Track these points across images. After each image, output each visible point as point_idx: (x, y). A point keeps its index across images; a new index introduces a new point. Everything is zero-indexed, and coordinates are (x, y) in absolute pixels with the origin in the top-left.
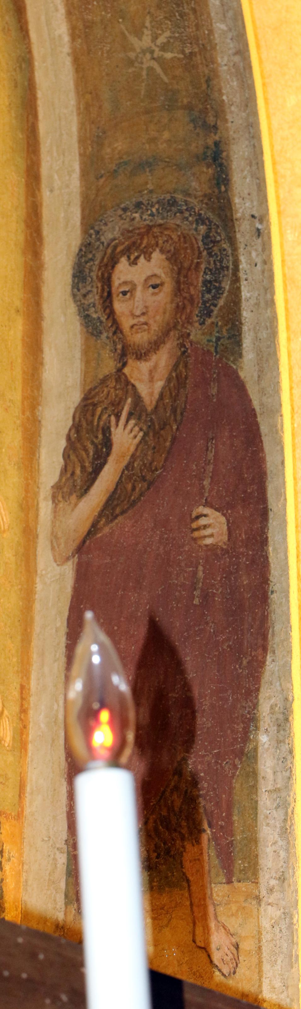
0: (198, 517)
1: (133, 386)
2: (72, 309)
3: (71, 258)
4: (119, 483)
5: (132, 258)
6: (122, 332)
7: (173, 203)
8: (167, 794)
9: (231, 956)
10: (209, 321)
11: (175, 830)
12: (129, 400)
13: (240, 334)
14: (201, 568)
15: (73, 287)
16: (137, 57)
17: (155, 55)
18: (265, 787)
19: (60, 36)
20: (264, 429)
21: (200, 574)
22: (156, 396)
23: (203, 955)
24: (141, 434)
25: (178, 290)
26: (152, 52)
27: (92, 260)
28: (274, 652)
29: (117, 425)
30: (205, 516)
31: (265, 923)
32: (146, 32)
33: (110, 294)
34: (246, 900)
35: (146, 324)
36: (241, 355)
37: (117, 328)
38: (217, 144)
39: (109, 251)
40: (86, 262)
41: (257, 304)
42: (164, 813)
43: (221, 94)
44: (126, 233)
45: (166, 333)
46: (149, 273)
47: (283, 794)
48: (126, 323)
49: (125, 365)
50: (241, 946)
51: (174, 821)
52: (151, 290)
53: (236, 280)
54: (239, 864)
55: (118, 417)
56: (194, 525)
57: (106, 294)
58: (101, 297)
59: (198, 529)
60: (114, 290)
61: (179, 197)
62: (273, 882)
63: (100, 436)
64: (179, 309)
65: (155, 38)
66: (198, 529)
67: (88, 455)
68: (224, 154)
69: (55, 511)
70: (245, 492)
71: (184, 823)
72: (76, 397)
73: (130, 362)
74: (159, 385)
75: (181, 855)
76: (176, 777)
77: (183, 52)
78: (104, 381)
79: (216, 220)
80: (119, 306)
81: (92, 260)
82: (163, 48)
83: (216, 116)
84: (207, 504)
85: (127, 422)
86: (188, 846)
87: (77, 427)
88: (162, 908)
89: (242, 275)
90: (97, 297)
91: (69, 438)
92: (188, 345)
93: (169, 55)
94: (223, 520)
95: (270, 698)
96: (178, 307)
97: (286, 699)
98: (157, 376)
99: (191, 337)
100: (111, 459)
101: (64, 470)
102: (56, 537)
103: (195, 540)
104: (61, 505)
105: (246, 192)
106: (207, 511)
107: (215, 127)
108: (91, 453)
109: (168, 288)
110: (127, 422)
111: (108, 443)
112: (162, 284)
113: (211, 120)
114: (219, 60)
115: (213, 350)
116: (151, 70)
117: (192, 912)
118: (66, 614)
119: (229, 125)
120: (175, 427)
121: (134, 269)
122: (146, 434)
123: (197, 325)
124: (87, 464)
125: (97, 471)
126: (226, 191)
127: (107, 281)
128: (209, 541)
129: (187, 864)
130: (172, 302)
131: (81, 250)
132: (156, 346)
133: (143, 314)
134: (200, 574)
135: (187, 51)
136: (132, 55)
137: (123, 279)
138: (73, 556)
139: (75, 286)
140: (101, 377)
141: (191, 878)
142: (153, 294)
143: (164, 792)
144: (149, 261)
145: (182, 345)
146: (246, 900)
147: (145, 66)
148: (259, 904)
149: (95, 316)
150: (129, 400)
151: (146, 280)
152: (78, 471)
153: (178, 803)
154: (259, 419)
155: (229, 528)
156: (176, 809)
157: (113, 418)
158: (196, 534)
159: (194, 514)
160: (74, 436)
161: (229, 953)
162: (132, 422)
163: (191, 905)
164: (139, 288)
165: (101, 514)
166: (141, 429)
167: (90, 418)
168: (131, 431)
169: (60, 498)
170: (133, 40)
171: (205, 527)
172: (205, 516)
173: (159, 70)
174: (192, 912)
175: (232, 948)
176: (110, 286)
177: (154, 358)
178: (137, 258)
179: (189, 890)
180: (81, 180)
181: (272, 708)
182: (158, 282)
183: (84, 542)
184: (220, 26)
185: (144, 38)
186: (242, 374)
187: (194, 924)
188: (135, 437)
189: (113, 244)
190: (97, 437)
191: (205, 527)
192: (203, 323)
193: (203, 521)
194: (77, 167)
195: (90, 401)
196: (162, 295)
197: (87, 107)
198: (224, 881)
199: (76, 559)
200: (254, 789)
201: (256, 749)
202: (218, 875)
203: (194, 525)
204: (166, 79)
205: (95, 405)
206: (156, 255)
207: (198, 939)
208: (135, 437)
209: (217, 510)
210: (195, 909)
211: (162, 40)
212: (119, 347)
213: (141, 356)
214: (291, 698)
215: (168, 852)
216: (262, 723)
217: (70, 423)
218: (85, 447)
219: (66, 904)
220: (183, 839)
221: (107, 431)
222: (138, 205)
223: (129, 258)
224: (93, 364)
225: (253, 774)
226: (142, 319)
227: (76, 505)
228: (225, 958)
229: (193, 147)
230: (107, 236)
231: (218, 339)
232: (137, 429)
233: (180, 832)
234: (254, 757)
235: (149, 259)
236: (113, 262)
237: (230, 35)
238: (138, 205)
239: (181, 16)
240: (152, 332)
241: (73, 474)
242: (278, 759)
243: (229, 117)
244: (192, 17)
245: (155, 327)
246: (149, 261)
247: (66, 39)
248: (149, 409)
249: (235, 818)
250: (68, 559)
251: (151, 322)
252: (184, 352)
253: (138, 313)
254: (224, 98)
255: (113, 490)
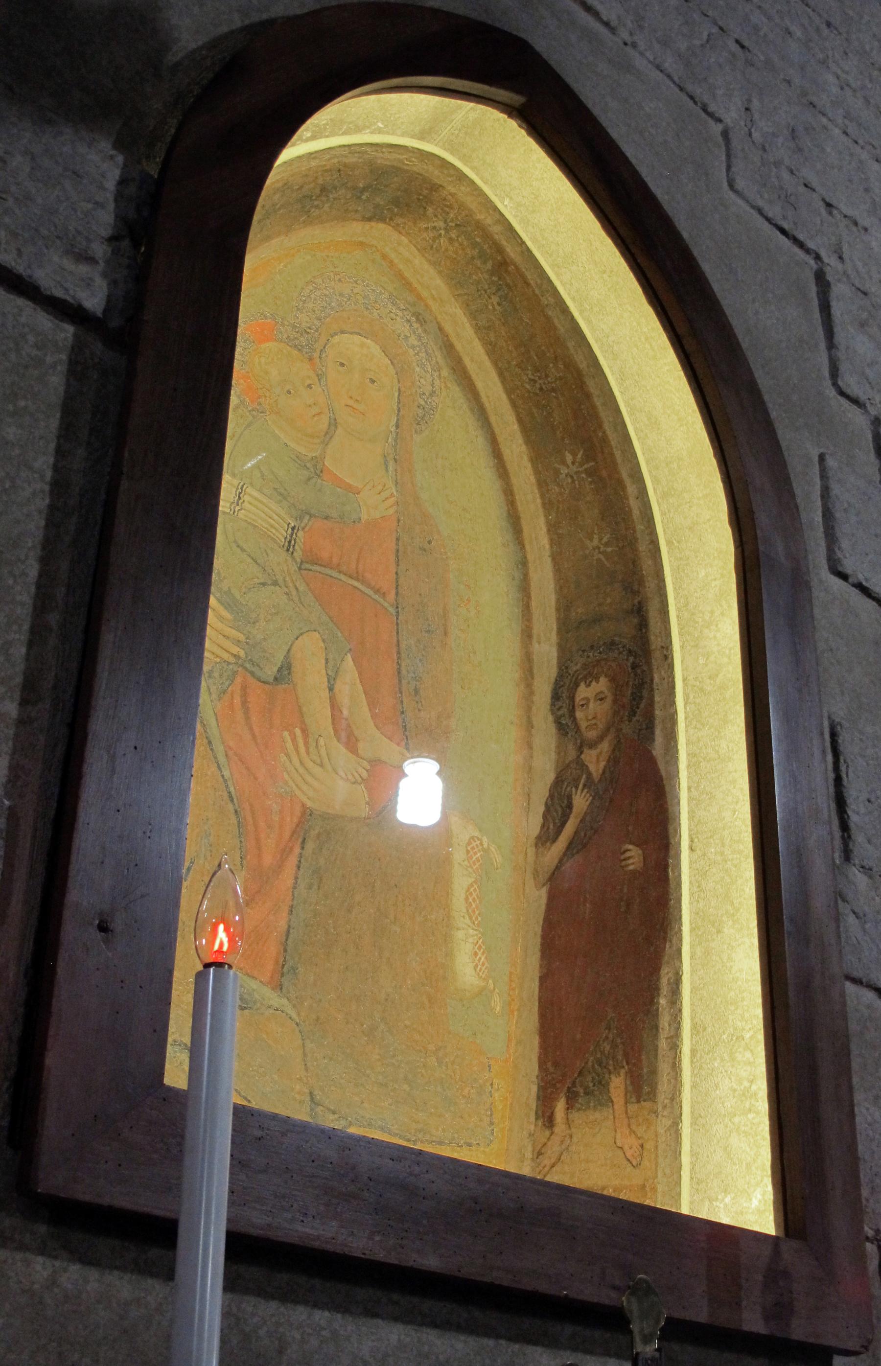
0: (625, 852)
1: (587, 766)
2: (551, 718)
3: (551, 685)
4: (576, 833)
5: (588, 682)
6: (580, 732)
7: (613, 643)
8: (601, 1042)
9: (638, 1152)
10: (634, 719)
11: (605, 1067)
12: (584, 776)
13: (654, 727)
14: (626, 886)
15: (551, 705)
16: (590, 553)
17: (601, 550)
18: (663, 1035)
19: (544, 546)
20: (667, 789)
21: (625, 890)
22: (601, 771)
23: (620, 1153)
24: (591, 798)
25: (615, 701)
26: (599, 548)
27: (563, 686)
28: (671, 941)
29: (576, 794)
30: (629, 850)
31: (661, 1131)
32: (595, 536)
33: (574, 707)
34: (648, 1114)
35: (595, 724)
36: (654, 740)
37: (578, 729)
38: (639, 603)
39: (574, 679)
40: (560, 688)
41: (664, 705)
42: (599, 1056)
43: (642, 570)
44: (585, 666)
45: (608, 729)
46: (599, 690)
47: (674, 1040)
48: (583, 725)
49: (582, 753)
50: (644, 1145)
51: (604, 1061)
52: (599, 702)
53: (652, 690)
54: (646, 1089)
55: (577, 788)
56: (622, 857)
57: (571, 708)
58: (568, 709)
59: (624, 860)
60: (576, 703)
61: (617, 639)
62: (667, 1101)
63: (566, 802)
64: (616, 713)
65: (601, 540)
66: (624, 860)
67: (557, 812)
68: (644, 608)
69: (537, 854)
70: (464, 1097)
71: (611, 1062)
72: (551, 777)
73: (585, 750)
74: (602, 764)
75: (608, 1084)
76: (607, 1031)
77: (617, 546)
78: (568, 766)
79: (640, 653)
80: (579, 714)
81: (563, 686)
82: (607, 544)
83: (639, 585)
84: (631, 843)
85: (582, 790)
86: (613, 1077)
87: (551, 796)
88: (596, 1121)
89: (655, 687)
90: (566, 710)
91: (546, 804)
92: (621, 736)
93: (609, 549)
94: (640, 852)
95: (668, 973)
96: (615, 711)
97: (677, 973)
98: (601, 759)
99: (624, 731)
100: (572, 816)
101: (543, 826)
102: (537, 871)
103: (622, 867)
104: (540, 850)
105: (658, 631)
106: (630, 847)
107: (639, 592)
108: (560, 813)
109: (609, 700)
110: (582, 790)
111: (570, 806)
112: (606, 697)
113: (636, 587)
114: (640, 548)
115: (636, 738)
116: (599, 560)
117: (614, 1122)
118: (541, 923)
119: (647, 589)
120: (611, 792)
121: (589, 689)
122: (594, 799)
123: (627, 722)
124: (557, 821)
125: (563, 824)
126: (646, 633)
127: (572, 698)
128: (631, 868)
129: (612, 1090)
130: (612, 708)
131: (556, 680)
132: (601, 738)
133: (594, 718)
134: (625, 890)
135: (621, 545)
136: (587, 552)
137: (582, 696)
138: (546, 883)
139: (553, 704)
140: (567, 762)
141: (614, 1100)
142: (600, 705)
143: (599, 1041)
144: (598, 683)
145: (618, 736)
146: (648, 1114)
147: (595, 558)
148: (657, 1117)
149: (564, 722)
150: (584, 776)
151: (597, 694)
152: (551, 826)
153: (608, 1048)
154: (665, 782)
155: (644, 857)
156: (606, 1052)
157: (574, 789)
158: (623, 863)
159: (622, 850)
160: (549, 802)
161: (637, 1150)
162: (586, 790)
163: (614, 1118)
164: (592, 701)
165: (565, 854)
166: (591, 795)
167: (559, 790)
168: (585, 796)
169: (540, 845)
170: (588, 542)
171: (629, 858)
172: (629, 850)
173: (603, 559)
174: (614, 1122)
175: (639, 1147)
176: (574, 702)
177: (600, 746)
178: (591, 682)
179: (613, 1109)
180: (557, 635)
181: (669, 980)
182: (603, 696)
183: (553, 873)
184: (640, 527)
185: (594, 540)
186: (654, 753)
187: (616, 1131)
188: (587, 800)
189: (576, 674)
190: (563, 802)
191: (629, 858)
192: (630, 721)
193: (628, 854)
194: (555, 627)
195: (560, 779)
196: (605, 704)
197: (561, 588)
198: (635, 1101)
199: (548, 885)
200: (656, 1036)
201: (657, 1010)
202: (631, 1097)
203: (622, 857)
204: (608, 565)
205: (563, 781)
206: (603, 680)
207: (618, 1141)
208: (587, 800)
209: (637, 846)
210: (616, 1120)
211: (605, 540)
212: (579, 741)
213: (592, 745)
214: (681, 973)
215: (600, 1082)
216: (662, 991)
217: (547, 795)
218: (555, 810)
219: (537, 1119)
220: (610, 1073)
221: (570, 798)
222: (592, 647)
223: (586, 682)
224: (562, 754)
225: (656, 1027)
226: (593, 722)
227: (549, 849)
228: (635, 1154)
229: (625, 607)
230: (574, 668)
231: (640, 730)
232: (588, 795)
233: (608, 1069)
234: (656, 1015)
235: (598, 682)
236: (577, 685)
237: (646, 532)
238: (592, 647)
239: (616, 523)
240: (599, 729)
241: (548, 828)
242: (672, 1016)
243: (647, 584)
244: (623, 524)
245: (601, 726)
246: (598, 683)
247: (547, 547)
248: (596, 781)
249: (643, 1057)
250: (544, 885)
251: (599, 723)
252: (619, 741)
253: (590, 718)
254: (644, 572)
255: (553, 867)
